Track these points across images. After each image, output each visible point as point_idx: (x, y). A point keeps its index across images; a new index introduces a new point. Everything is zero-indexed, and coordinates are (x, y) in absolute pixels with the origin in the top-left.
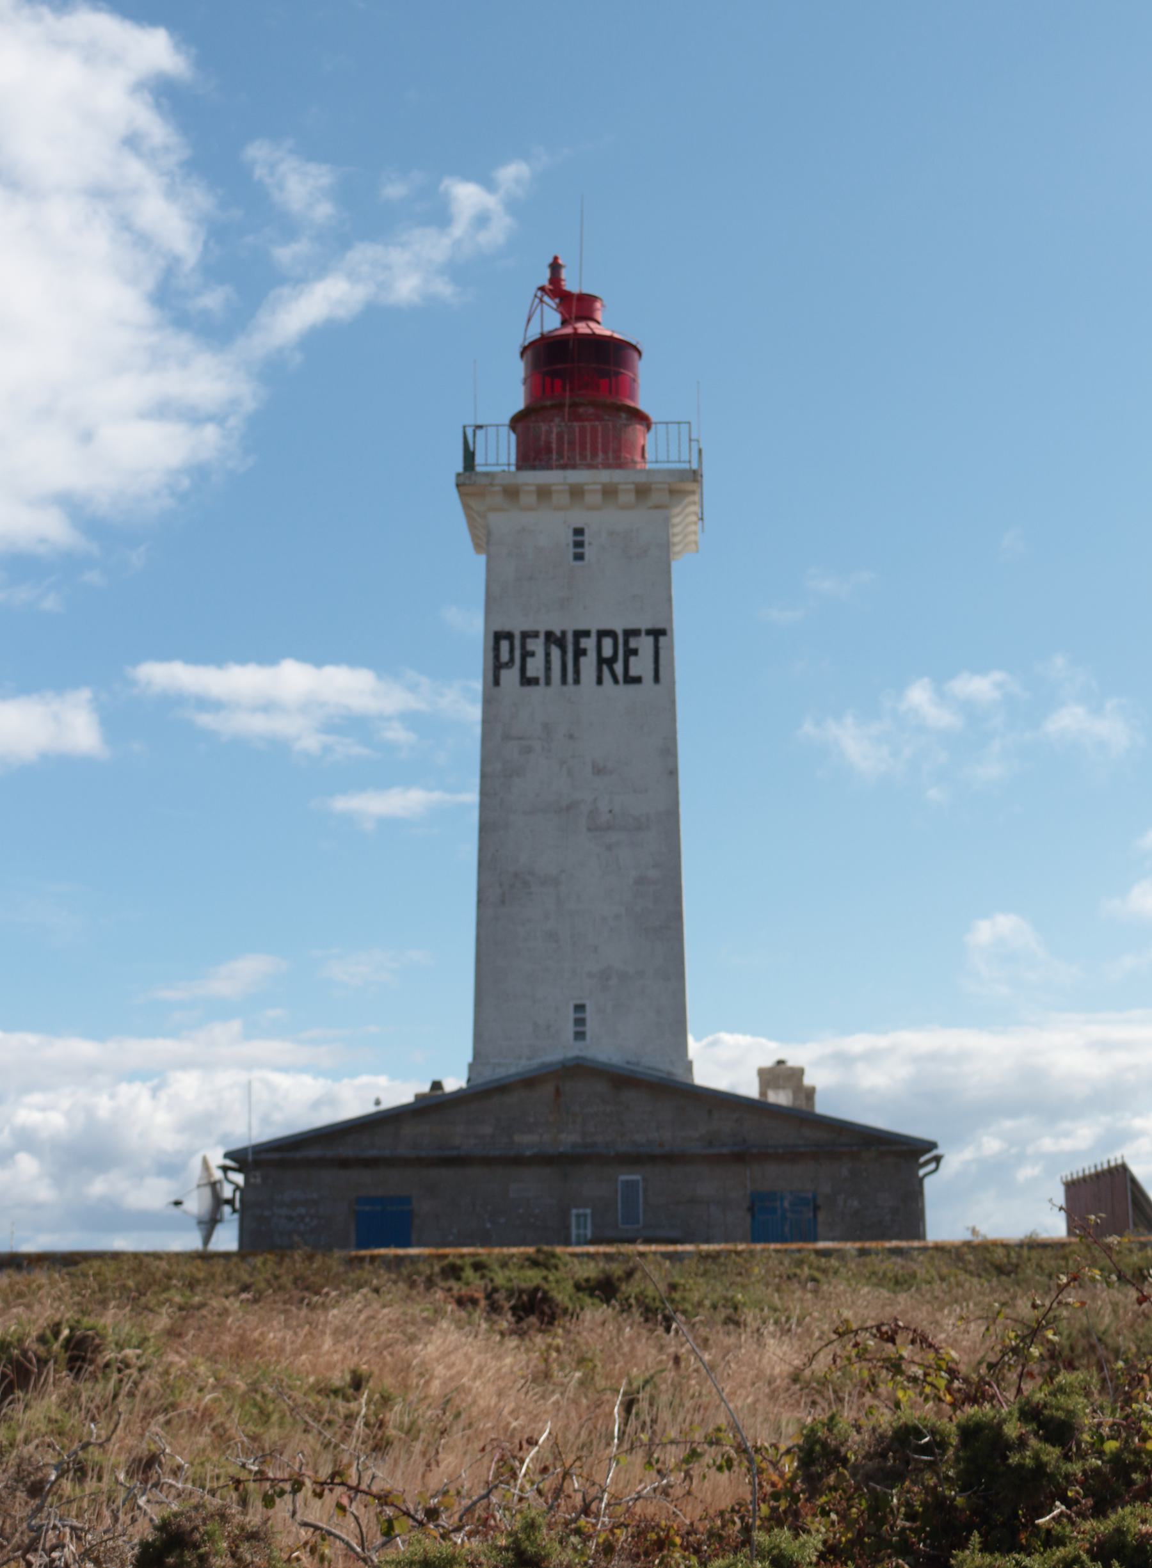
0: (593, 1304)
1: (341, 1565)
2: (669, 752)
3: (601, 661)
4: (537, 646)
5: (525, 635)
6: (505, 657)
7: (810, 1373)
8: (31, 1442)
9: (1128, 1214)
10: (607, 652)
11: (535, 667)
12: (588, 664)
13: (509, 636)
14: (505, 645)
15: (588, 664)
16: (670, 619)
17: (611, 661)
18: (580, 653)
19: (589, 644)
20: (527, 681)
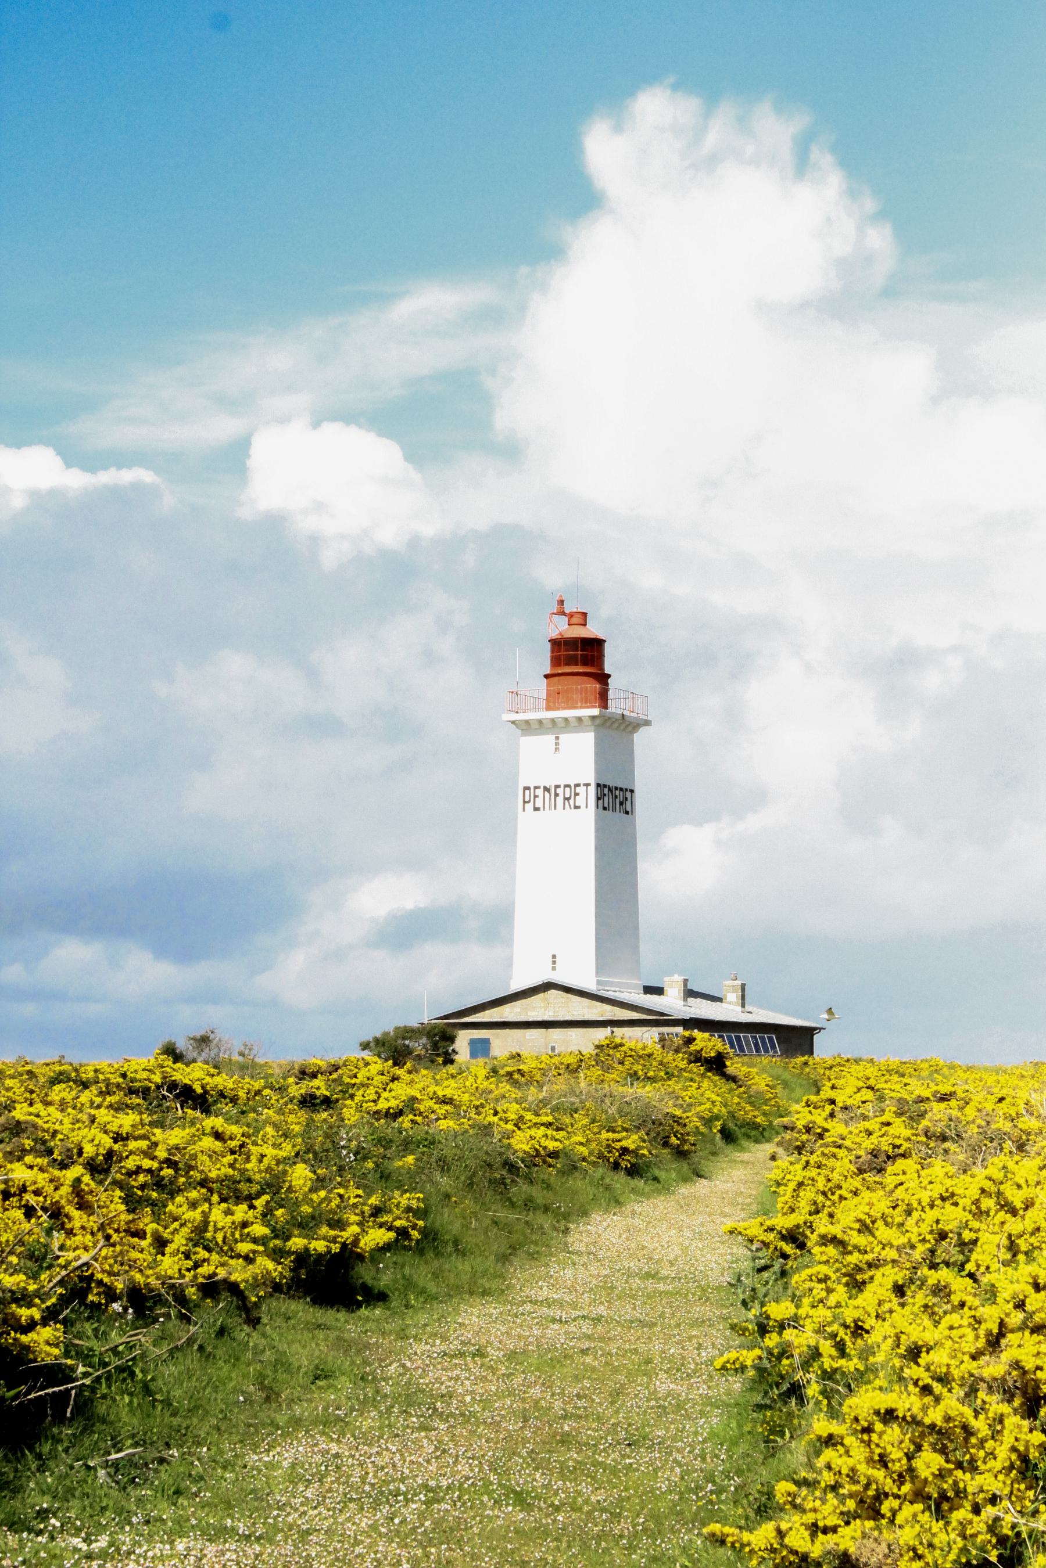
0: (634, 1191)
1: (1043, 1234)
2: (597, 960)
3: (565, 799)
4: (540, 792)
5: (536, 788)
6: (527, 799)
7: (903, 1488)
8: (622, 1148)
9: (454, 1023)
10: (567, 796)
11: (539, 803)
12: (560, 799)
13: (528, 788)
14: (527, 792)
15: (560, 799)
16: (597, 815)
17: (568, 799)
18: (557, 795)
19: (560, 791)
20: (536, 809)
